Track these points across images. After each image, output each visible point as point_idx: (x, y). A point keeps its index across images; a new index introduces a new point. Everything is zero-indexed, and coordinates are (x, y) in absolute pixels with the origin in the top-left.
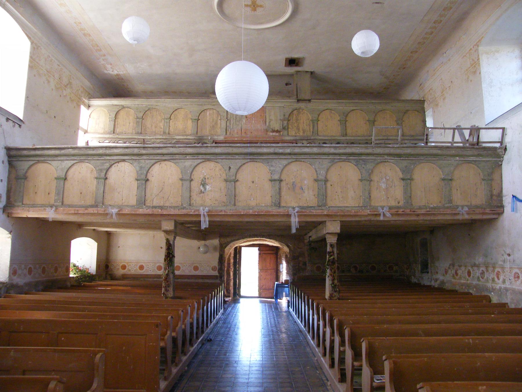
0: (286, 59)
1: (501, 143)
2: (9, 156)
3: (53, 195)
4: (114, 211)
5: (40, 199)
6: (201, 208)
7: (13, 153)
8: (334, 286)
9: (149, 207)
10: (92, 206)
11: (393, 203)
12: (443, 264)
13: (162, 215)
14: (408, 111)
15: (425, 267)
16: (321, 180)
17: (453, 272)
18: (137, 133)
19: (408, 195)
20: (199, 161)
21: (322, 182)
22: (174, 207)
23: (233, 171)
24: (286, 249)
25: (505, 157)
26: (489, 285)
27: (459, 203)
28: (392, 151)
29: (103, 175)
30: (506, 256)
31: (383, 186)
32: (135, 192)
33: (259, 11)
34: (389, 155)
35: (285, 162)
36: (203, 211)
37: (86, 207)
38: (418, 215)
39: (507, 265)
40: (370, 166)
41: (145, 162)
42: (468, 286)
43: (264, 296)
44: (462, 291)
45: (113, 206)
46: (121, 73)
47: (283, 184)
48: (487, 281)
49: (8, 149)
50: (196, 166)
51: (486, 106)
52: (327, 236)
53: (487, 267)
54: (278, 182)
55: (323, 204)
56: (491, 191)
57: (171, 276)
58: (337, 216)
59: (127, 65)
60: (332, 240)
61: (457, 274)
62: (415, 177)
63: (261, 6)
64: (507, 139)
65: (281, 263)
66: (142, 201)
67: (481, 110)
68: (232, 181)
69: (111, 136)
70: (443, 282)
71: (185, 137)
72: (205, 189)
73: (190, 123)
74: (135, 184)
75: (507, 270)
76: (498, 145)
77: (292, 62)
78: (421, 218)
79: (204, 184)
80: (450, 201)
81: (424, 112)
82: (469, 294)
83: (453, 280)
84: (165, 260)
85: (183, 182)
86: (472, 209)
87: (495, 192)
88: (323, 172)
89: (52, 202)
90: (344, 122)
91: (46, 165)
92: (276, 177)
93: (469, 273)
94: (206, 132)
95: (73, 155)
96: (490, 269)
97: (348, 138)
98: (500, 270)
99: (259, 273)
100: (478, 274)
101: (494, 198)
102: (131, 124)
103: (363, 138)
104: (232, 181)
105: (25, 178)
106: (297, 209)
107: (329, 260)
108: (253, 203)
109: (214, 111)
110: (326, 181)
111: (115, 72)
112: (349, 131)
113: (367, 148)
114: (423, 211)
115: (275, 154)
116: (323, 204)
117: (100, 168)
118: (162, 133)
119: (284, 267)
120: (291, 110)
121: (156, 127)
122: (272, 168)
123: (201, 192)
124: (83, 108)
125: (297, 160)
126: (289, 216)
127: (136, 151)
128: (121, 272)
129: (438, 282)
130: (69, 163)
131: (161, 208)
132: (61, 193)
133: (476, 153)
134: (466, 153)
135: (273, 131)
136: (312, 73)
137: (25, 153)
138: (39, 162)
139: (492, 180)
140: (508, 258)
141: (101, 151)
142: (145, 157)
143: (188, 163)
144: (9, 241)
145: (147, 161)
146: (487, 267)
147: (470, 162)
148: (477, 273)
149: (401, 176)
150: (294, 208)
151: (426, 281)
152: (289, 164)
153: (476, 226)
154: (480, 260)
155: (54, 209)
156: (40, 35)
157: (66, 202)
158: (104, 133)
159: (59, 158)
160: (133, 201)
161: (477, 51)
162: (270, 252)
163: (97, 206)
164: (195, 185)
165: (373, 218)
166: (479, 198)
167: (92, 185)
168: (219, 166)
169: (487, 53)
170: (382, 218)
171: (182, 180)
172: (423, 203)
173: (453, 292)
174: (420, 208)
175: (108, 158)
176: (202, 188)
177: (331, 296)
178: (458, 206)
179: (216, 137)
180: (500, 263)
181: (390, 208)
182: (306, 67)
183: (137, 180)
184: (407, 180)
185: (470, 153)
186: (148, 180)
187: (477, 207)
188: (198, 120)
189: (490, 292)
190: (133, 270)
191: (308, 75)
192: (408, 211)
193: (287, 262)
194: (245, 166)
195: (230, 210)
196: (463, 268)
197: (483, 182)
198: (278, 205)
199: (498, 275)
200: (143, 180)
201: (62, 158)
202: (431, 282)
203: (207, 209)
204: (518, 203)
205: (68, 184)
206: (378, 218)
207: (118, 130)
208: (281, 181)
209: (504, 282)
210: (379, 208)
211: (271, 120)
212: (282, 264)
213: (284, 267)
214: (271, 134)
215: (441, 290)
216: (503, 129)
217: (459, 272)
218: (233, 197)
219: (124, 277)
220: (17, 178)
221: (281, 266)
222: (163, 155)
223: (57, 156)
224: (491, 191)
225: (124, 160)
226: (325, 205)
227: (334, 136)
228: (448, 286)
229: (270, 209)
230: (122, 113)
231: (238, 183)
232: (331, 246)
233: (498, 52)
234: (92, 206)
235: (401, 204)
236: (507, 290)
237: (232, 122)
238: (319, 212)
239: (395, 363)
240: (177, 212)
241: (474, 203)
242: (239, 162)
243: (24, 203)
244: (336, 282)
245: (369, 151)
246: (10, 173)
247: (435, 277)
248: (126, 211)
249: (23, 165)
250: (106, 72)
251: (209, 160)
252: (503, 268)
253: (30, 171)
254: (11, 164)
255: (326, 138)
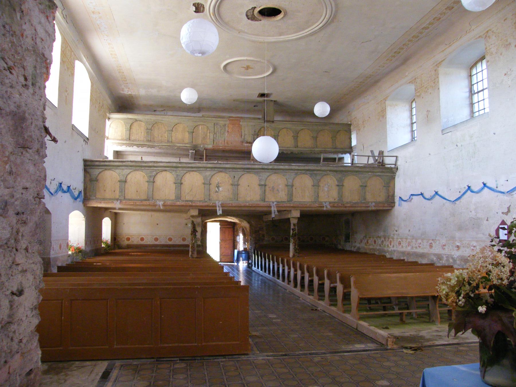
0: (259, 94)
1: (395, 165)
2: (85, 165)
3: (117, 192)
4: (161, 203)
5: (108, 195)
6: (217, 202)
7: (89, 163)
8: (295, 250)
9: (183, 201)
10: (145, 200)
11: (332, 200)
12: (359, 236)
13: (192, 206)
14: (339, 131)
15: (347, 238)
16: (290, 186)
17: (366, 241)
18: (148, 141)
19: (341, 195)
20: (215, 172)
21: (290, 187)
22: (200, 201)
23: (236, 179)
24: (245, 224)
25: (397, 173)
26: (386, 249)
27: (370, 201)
28: (332, 168)
29: (152, 180)
30: (395, 232)
31: (326, 189)
32: (174, 192)
33: (250, 70)
34: (330, 171)
35: (268, 174)
36: (218, 204)
37: (142, 201)
38: (346, 207)
39: (395, 237)
40: (318, 177)
41: (180, 172)
42: (374, 250)
43: (224, 261)
44: (370, 253)
45: (160, 200)
46: (133, 93)
47: (267, 187)
48: (385, 246)
49: (85, 161)
50: (213, 176)
51: (388, 139)
52: (291, 219)
53: (385, 238)
54: (264, 187)
55: (290, 200)
56: (388, 193)
57: (196, 244)
58: (298, 207)
59: (141, 90)
60: (294, 221)
61: (368, 242)
62: (345, 184)
63: (252, 68)
64: (399, 163)
65: (238, 235)
66: (178, 197)
67: (385, 142)
68: (236, 185)
69: (127, 142)
70: (359, 248)
71: (184, 145)
72: (219, 190)
73: (187, 135)
74: (174, 186)
75: (395, 239)
76: (393, 166)
77: (262, 95)
78: (347, 209)
79: (218, 187)
80: (365, 199)
81: (351, 132)
82: (374, 254)
83: (366, 247)
84: (191, 234)
85: (206, 185)
86: (377, 203)
87: (391, 194)
88: (290, 180)
89: (117, 197)
90: (296, 137)
91: (111, 172)
92: (263, 183)
93: (375, 242)
94: (199, 141)
95: (131, 166)
96: (387, 239)
97: (299, 149)
98: (392, 240)
99: (220, 243)
100: (380, 243)
101: (390, 197)
102: (143, 134)
103: (309, 149)
104: (236, 185)
105: (97, 180)
106: (275, 203)
107: (293, 234)
108: (248, 199)
109: (205, 126)
110: (292, 186)
111: (130, 93)
112: (299, 144)
113: (317, 166)
114: (349, 205)
115: (263, 169)
116: (290, 200)
117: (150, 175)
118: (166, 141)
119: (241, 238)
120: (259, 128)
121: (161, 137)
122: (260, 178)
123: (216, 192)
124: (107, 120)
125: (275, 173)
126: (271, 207)
127: (175, 165)
128: (126, 243)
129: (356, 248)
130: (128, 171)
131: (191, 201)
132: (122, 190)
133: (381, 170)
134: (375, 171)
135: (247, 143)
136: (275, 101)
137: (97, 163)
138: (106, 169)
139: (389, 187)
140: (396, 233)
141: (150, 164)
142: (180, 169)
143: (208, 173)
144: (84, 223)
145: (182, 172)
146: (385, 238)
147: (377, 176)
148: (379, 241)
149: (337, 183)
150: (273, 202)
151: (348, 247)
152: (270, 175)
153: (377, 215)
154: (381, 234)
155: (119, 202)
156: (95, 76)
157: (126, 197)
158: (122, 140)
159: (121, 168)
160: (173, 197)
161: (385, 103)
162: (228, 226)
163: (149, 200)
164: (213, 188)
165: (320, 209)
166: (381, 197)
167: (145, 186)
168: (227, 175)
169: (391, 106)
170: (325, 209)
171: (204, 184)
172: (349, 200)
173: (366, 253)
174: (347, 203)
175: (155, 168)
176: (217, 189)
177: (294, 256)
178: (369, 202)
179: (206, 146)
180: (392, 235)
181: (330, 203)
182: (272, 98)
183: (175, 183)
184: (340, 186)
185: (378, 170)
186: (182, 184)
187: (380, 203)
188: (193, 132)
189: (386, 253)
190: (136, 241)
191: (272, 103)
192: (340, 205)
193: (244, 235)
194: (243, 176)
195: (234, 203)
196: (371, 239)
197: (384, 188)
198: (264, 200)
199: (391, 242)
200: (179, 184)
201: (123, 168)
202: (351, 248)
203: (220, 203)
204: (402, 202)
205: (127, 185)
206: (322, 209)
207: (132, 138)
208: (265, 185)
209: (393, 246)
210: (324, 203)
211: (245, 135)
212: (239, 236)
213: (241, 238)
214: (246, 144)
215: (357, 253)
216: (397, 157)
217: (369, 241)
218: (236, 195)
219: (129, 247)
220: (91, 180)
221: (238, 237)
222: (192, 167)
223: (119, 166)
224: (388, 193)
225: (166, 170)
226: (291, 200)
227: (289, 147)
228: (362, 250)
229: (259, 203)
230: (135, 124)
231: (239, 187)
232: (294, 225)
233: (397, 105)
234: (145, 200)
235: (336, 200)
236: (394, 251)
237: (218, 135)
238: (288, 205)
239: (341, 274)
240: (201, 204)
241: (378, 201)
242: (240, 173)
243: (97, 197)
244: (297, 246)
245: (319, 168)
246: (85, 177)
247: (354, 244)
248: (169, 203)
249: (95, 172)
250: (122, 92)
251: (221, 171)
252: (393, 238)
253: (100, 175)
254: (86, 171)
255: (284, 149)
